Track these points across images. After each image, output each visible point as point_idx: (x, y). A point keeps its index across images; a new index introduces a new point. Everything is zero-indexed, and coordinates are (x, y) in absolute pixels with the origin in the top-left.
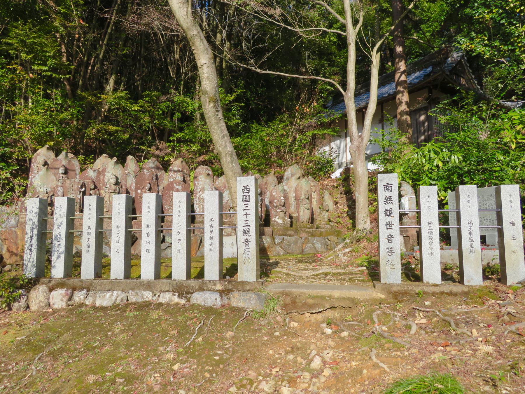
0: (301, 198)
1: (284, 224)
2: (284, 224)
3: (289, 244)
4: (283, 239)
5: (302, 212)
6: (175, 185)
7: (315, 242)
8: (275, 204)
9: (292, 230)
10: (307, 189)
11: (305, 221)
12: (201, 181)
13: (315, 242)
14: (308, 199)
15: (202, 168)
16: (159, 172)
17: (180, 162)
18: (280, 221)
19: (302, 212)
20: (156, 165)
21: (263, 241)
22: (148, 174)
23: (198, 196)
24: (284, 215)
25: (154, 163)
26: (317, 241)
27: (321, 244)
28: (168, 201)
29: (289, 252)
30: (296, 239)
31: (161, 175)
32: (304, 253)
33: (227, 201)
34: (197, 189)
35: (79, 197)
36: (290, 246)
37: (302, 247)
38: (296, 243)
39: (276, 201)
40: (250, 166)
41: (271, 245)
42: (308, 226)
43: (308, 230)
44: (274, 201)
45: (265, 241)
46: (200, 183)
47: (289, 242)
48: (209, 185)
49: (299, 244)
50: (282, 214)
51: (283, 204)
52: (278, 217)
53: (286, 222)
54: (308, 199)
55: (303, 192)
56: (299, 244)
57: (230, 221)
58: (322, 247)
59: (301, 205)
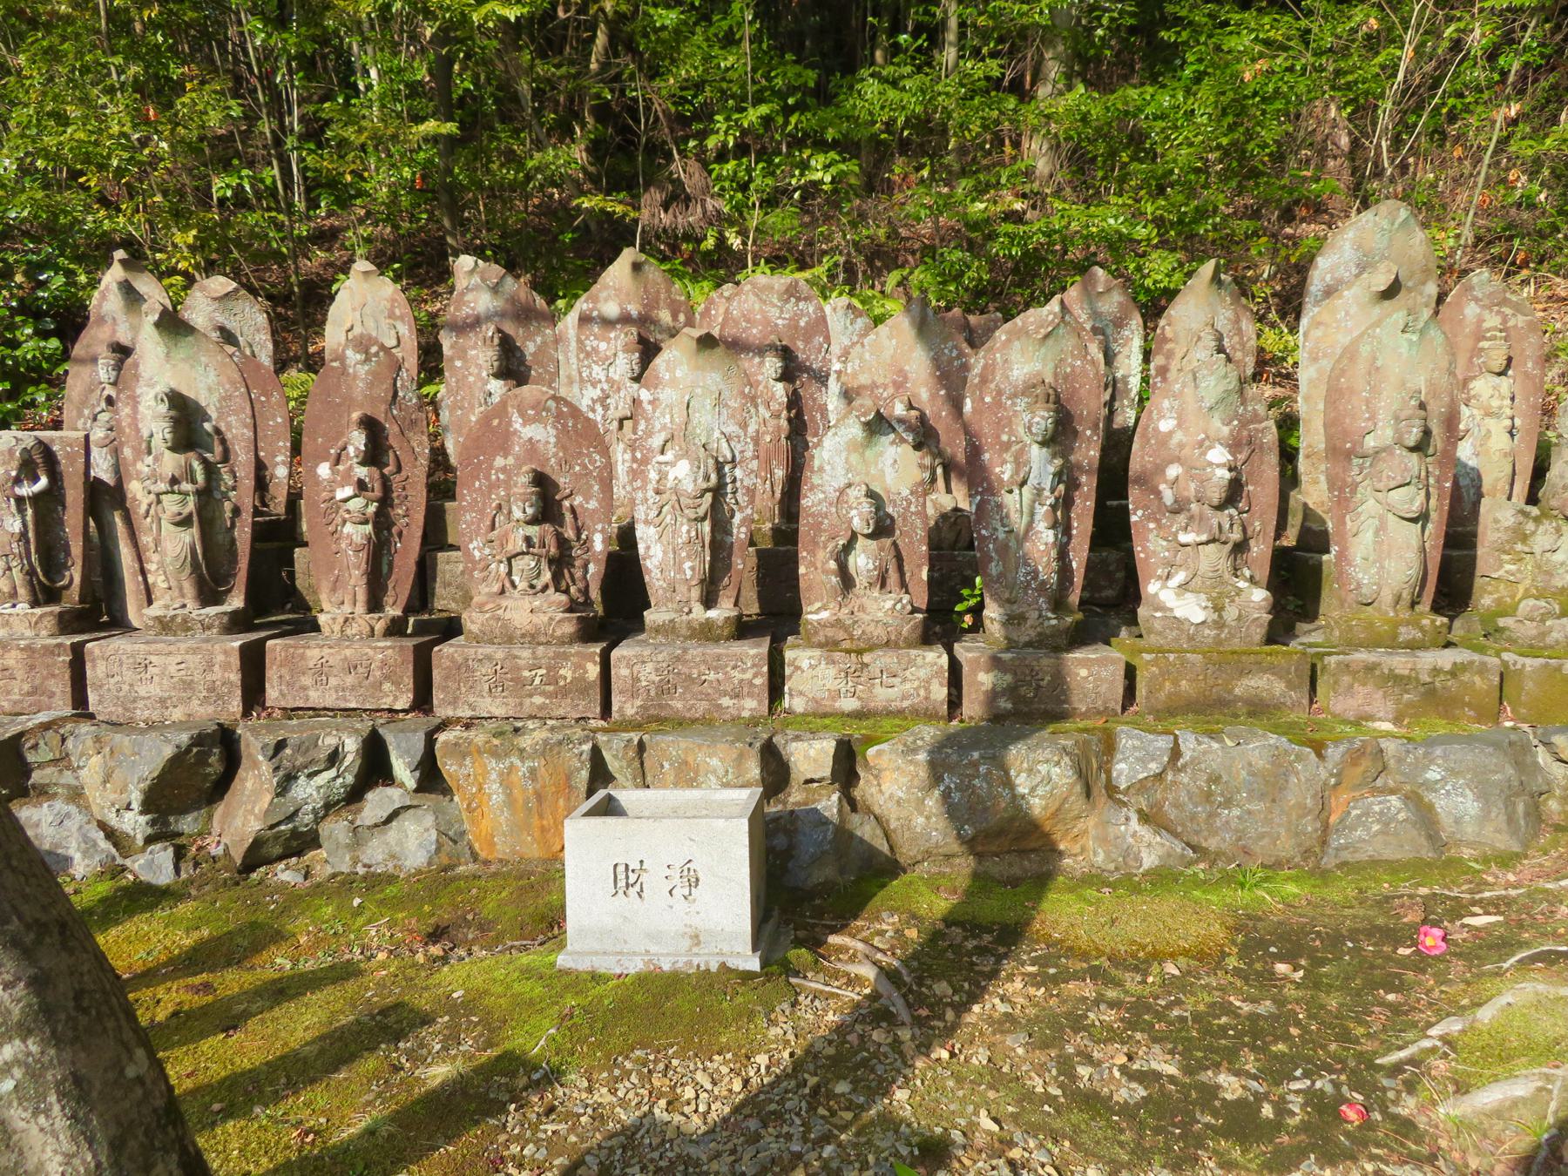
0: (1370, 442)
1: (1220, 624)
2: (1220, 624)
3: (1215, 792)
4: (1176, 753)
5: (1368, 536)
6: (517, 423)
7: (1433, 774)
8: (1168, 497)
9: (1272, 669)
10: (1420, 382)
11: (1387, 597)
12: (674, 382)
13: (1433, 774)
14: (1419, 448)
15: (759, 291)
16: (530, 337)
17: (627, 269)
18: (1192, 609)
19: (1368, 536)
20: (513, 300)
21: (1009, 784)
22: (363, 370)
23: (653, 475)
24: (1225, 565)
25: (495, 290)
26: (1453, 772)
27: (1483, 796)
28: (482, 512)
29: (1212, 844)
30: (1277, 757)
31: (541, 350)
32: (1329, 861)
33: (842, 492)
34: (649, 433)
35: (16, 526)
36: (1228, 803)
37: (1323, 808)
38: (1272, 784)
39: (1173, 471)
40: (1141, 232)
41: (1077, 803)
42: (1406, 634)
43: (1400, 662)
44: (1160, 470)
45: (1022, 784)
46: (667, 395)
47: (1215, 779)
48: (719, 401)
49: (1298, 792)
50: (1213, 558)
51: (1216, 495)
52: (1180, 577)
53: (1231, 613)
54: (1419, 448)
55: (1389, 402)
56: (1298, 792)
57: (838, 623)
58: (1485, 817)
59: (1364, 490)
